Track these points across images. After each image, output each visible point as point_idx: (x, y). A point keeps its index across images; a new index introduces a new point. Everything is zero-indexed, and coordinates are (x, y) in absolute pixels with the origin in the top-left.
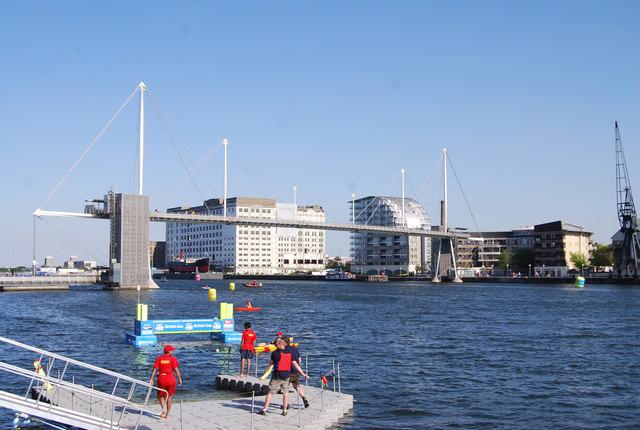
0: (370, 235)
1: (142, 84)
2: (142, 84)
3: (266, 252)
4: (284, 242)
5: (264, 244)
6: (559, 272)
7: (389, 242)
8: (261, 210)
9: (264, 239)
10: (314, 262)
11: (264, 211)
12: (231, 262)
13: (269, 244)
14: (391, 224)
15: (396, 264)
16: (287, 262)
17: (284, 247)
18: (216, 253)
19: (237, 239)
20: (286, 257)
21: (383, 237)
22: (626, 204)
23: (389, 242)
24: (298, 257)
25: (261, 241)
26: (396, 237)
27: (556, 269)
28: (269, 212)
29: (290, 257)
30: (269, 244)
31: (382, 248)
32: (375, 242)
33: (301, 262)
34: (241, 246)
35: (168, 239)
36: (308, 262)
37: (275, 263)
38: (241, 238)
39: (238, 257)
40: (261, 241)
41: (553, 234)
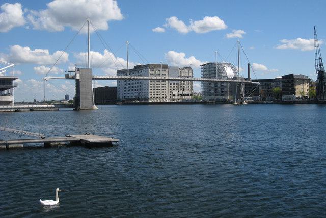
0: (210, 83)
1: (58, 190)
2: (58, 190)
3: (164, 91)
4: (173, 86)
5: (157, 87)
6: (292, 98)
7: (219, 85)
8: (155, 70)
9: (157, 84)
10: (188, 95)
11: (163, 71)
12: (147, 96)
13: (165, 87)
14: (220, 76)
15: (216, 95)
16: (174, 95)
17: (172, 88)
18: (140, 91)
19: (149, 87)
20: (174, 93)
21: (216, 82)
22: (320, 65)
23: (219, 85)
24: (180, 93)
25: (161, 88)
26: (222, 82)
27: (291, 96)
28: (165, 71)
29: (175, 93)
30: (165, 87)
31: (222, 87)
32: (213, 85)
33: (181, 95)
34: (151, 91)
35: (118, 85)
36: (185, 95)
37: (168, 96)
38: (151, 84)
39: (150, 88)
40: (161, 88)
41: (289, 80)
